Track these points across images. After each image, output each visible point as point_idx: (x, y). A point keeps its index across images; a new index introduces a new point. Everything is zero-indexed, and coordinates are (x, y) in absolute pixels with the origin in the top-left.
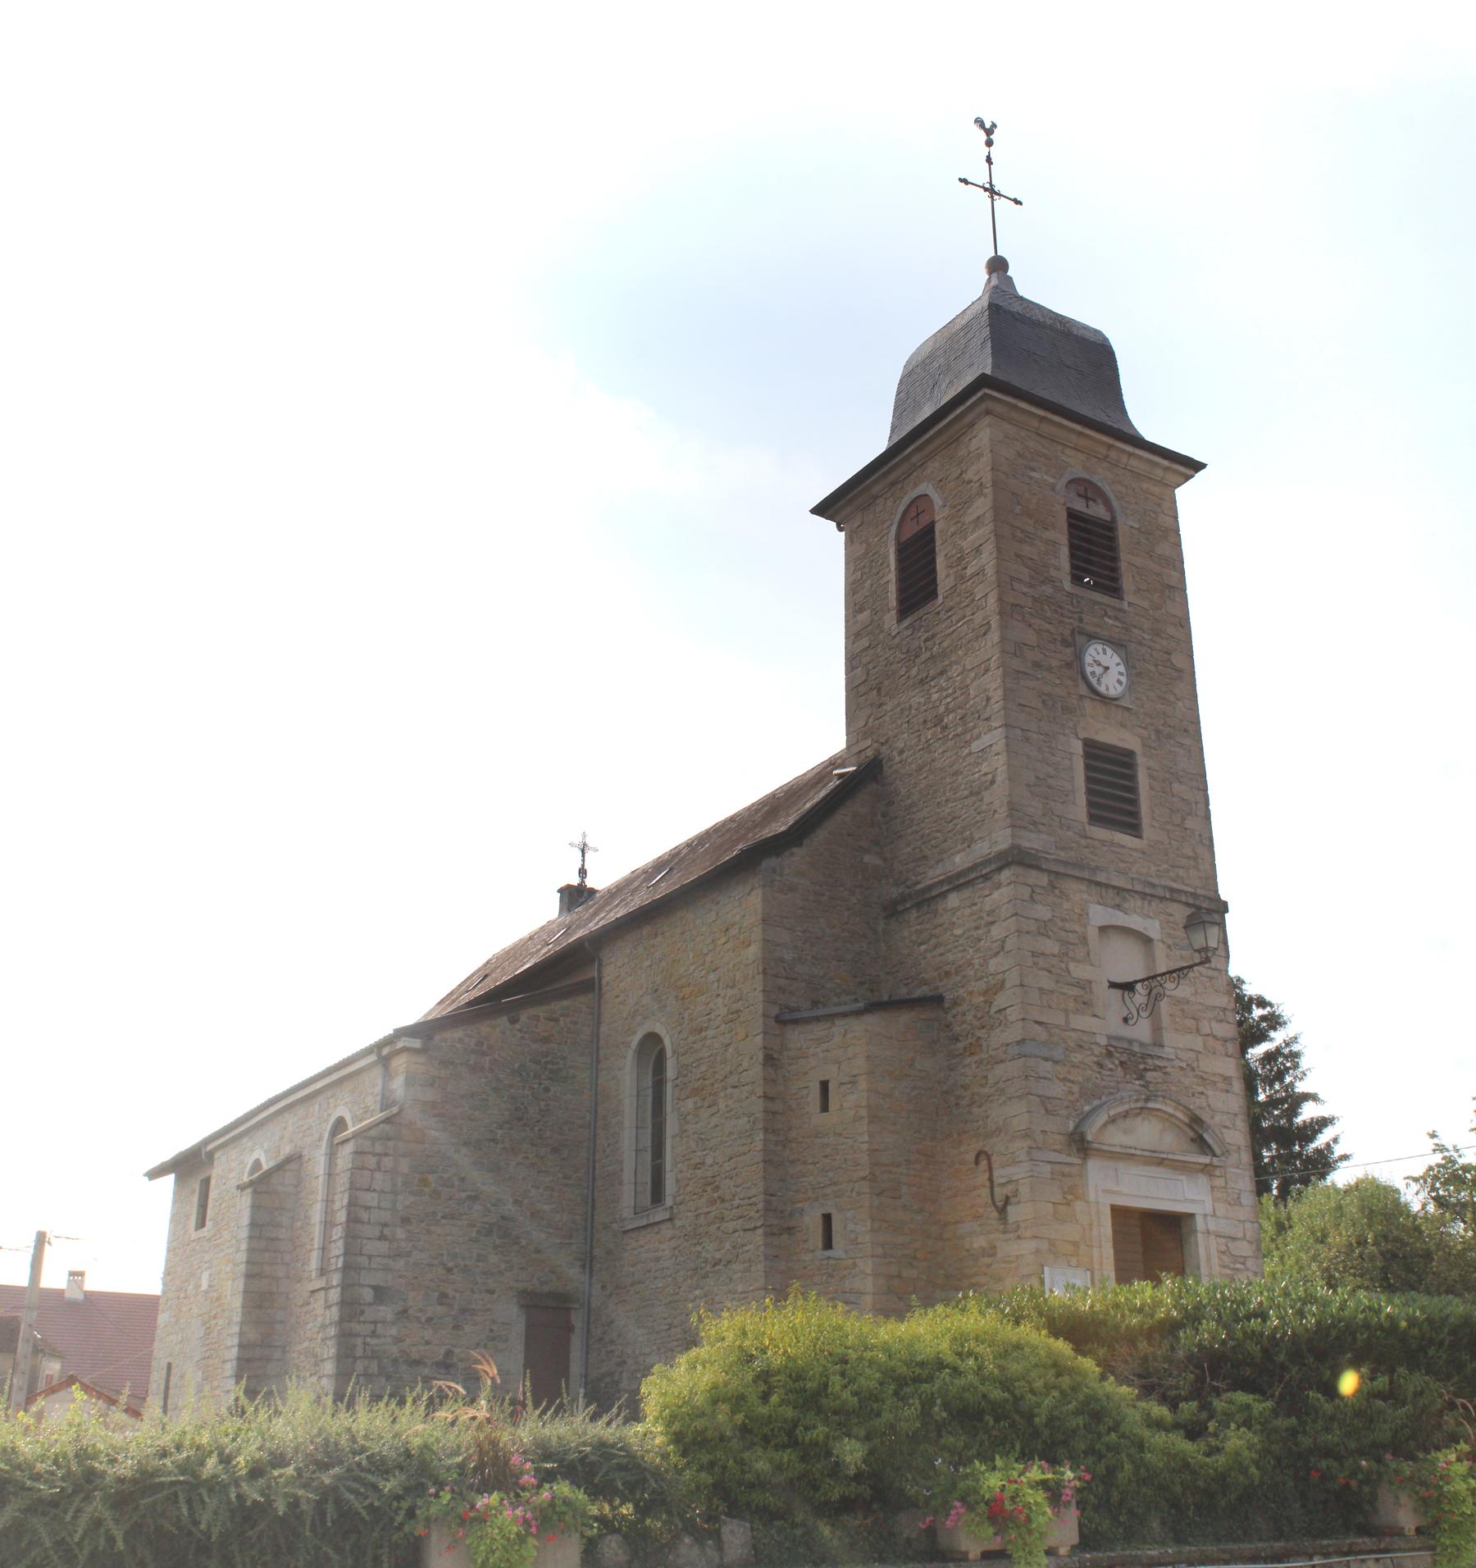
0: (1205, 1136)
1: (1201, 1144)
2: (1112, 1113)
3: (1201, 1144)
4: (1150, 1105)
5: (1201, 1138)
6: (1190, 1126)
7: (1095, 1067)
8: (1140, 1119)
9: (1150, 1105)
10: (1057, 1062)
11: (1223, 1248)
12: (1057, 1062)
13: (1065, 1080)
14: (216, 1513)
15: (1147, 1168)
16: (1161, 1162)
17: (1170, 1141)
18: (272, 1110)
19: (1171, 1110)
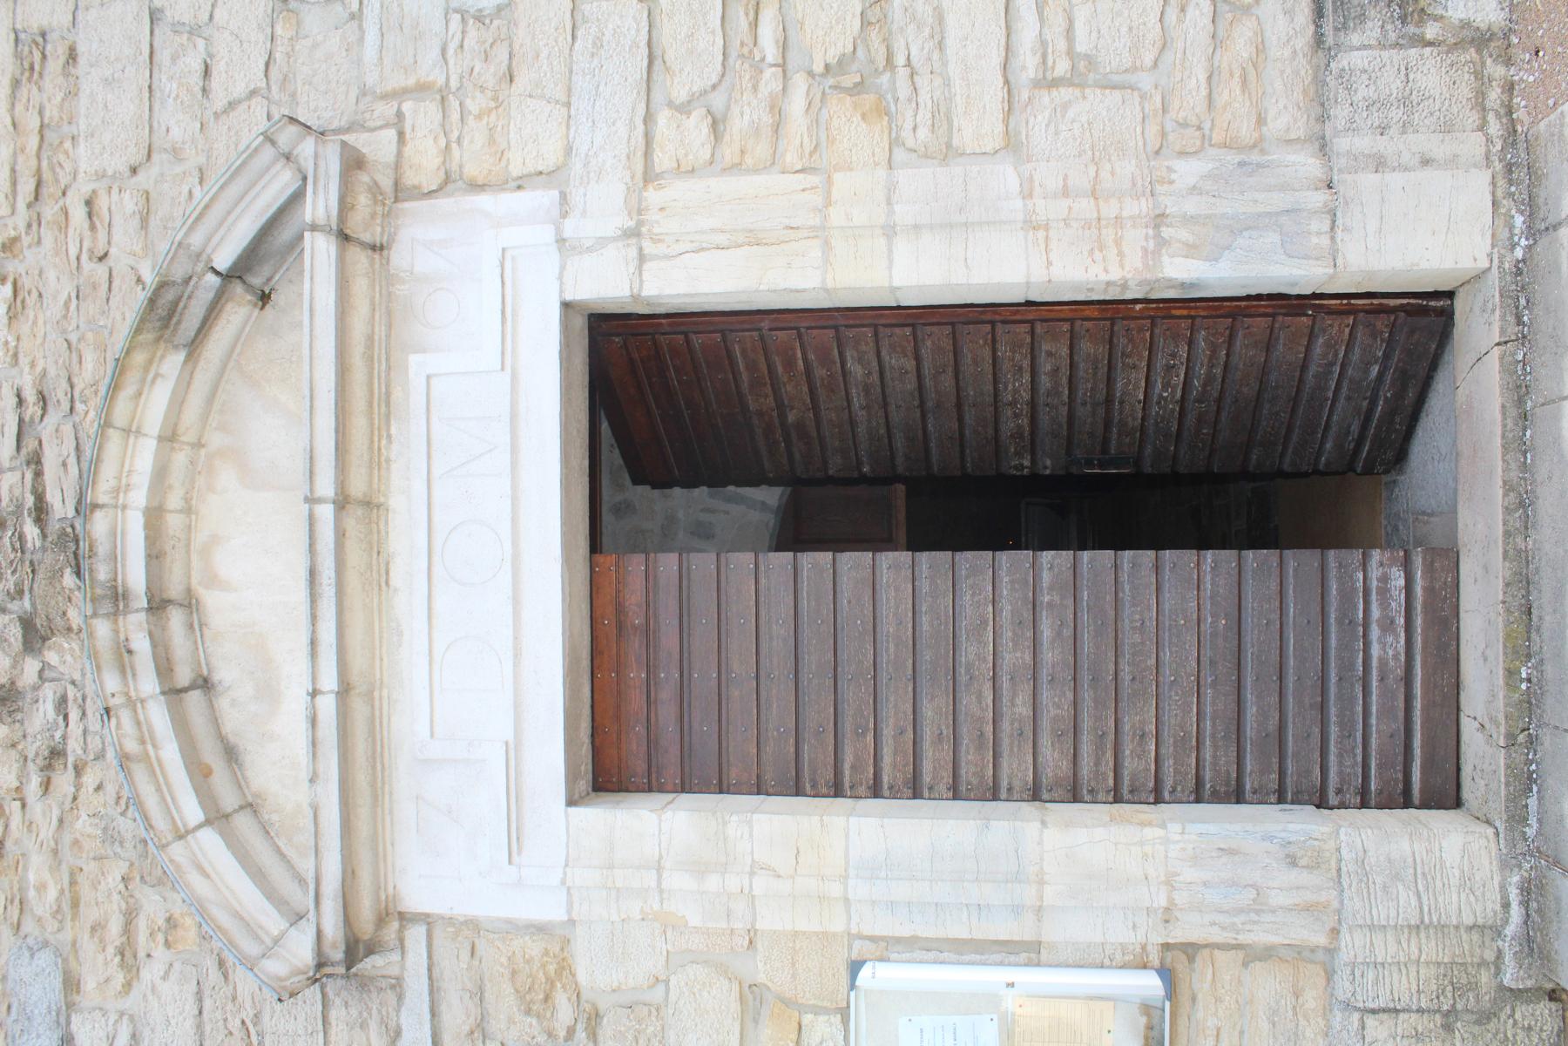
0: (223, 261)
1: (256, 272)
2: (192, 812)
3: (256, 272)
4: (136, 577)
5: (236, 274)
6: (194, 346)
7: (64, 781)
8: (212, 600)
9: (136, 577)
10: (71, 984)
11: (697, 127)
12: (71, 984)
13: (127, 956)
14: (897, 100)
15: (396, 578)
16: (357, 505)
17: (276, 414)
18: (512, 763)
19: (144, 456)
